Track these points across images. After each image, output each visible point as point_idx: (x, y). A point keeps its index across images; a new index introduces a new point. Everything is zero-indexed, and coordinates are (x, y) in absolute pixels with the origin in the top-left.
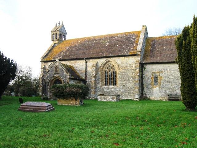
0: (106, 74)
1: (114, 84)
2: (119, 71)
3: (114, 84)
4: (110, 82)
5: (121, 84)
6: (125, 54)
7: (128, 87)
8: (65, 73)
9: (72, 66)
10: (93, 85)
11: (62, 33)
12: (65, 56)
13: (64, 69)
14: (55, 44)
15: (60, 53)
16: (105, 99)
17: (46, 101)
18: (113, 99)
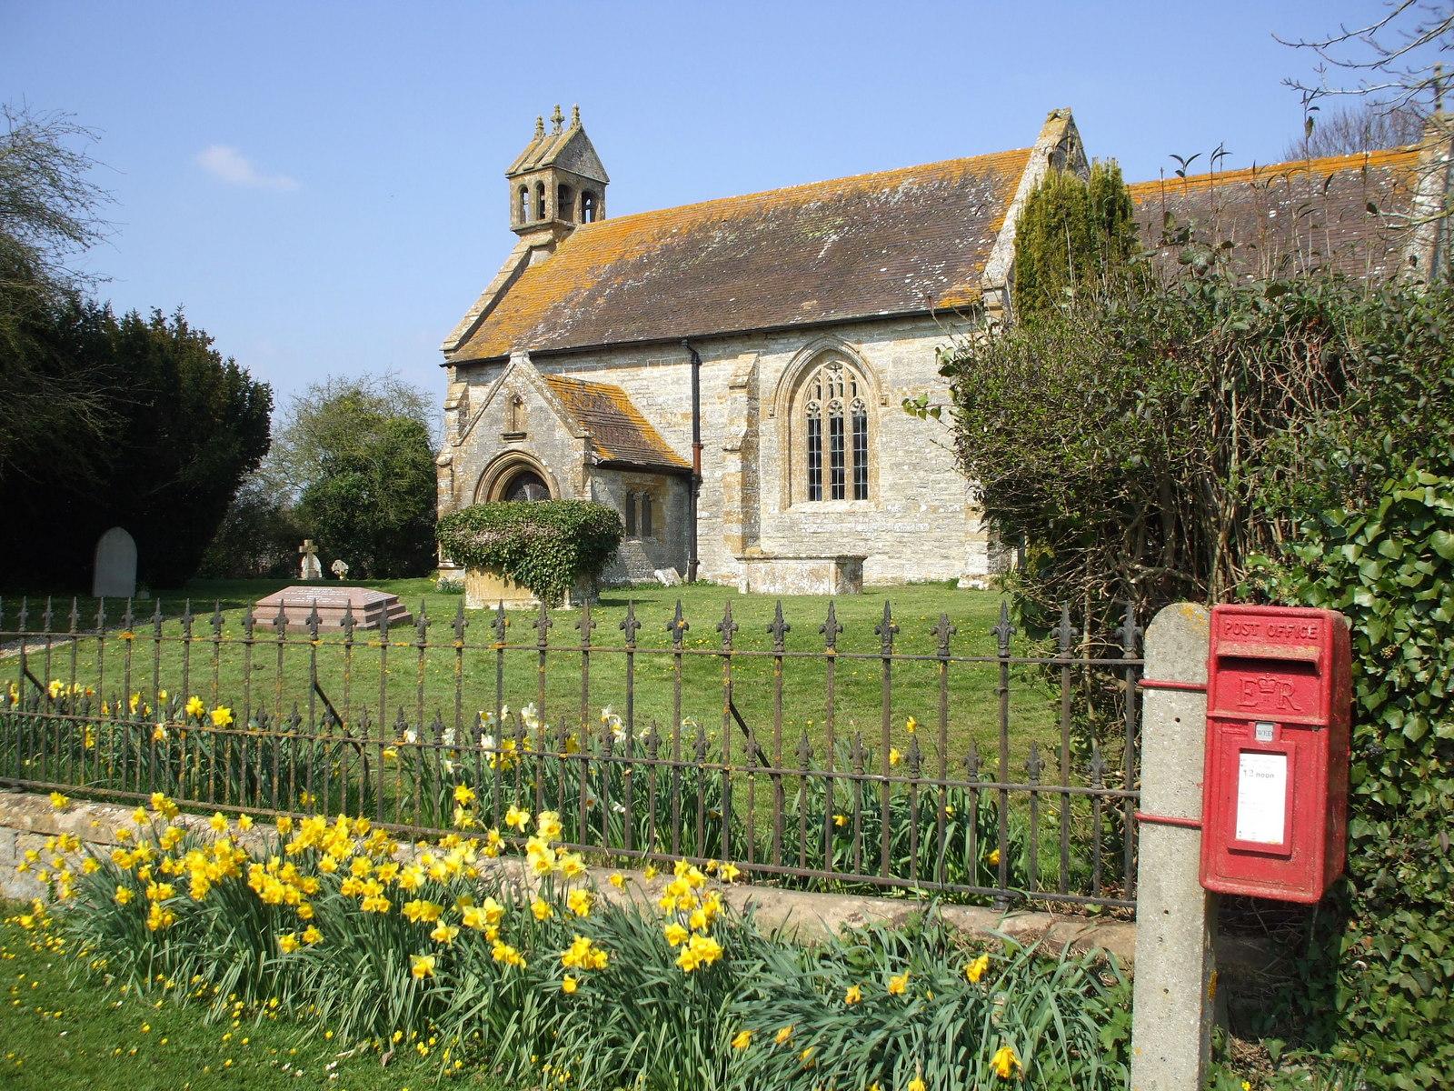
0: (811, 431)
1: (857, 488)
2: (884, 409)
3: (861, 493)
4: (838, 477)
5: (892, 487)
6: (912, 307)
7: (935, 510)
8: (561, 433)
9: (616, 390)
10: (731, 499)
11: (572, 181)
12: (577, 326)
13: (558, 412)
14: (532, 248)
15: (557, 311)
16: (773, 583)
17: (1210, 1012)
18: (816, 576)
